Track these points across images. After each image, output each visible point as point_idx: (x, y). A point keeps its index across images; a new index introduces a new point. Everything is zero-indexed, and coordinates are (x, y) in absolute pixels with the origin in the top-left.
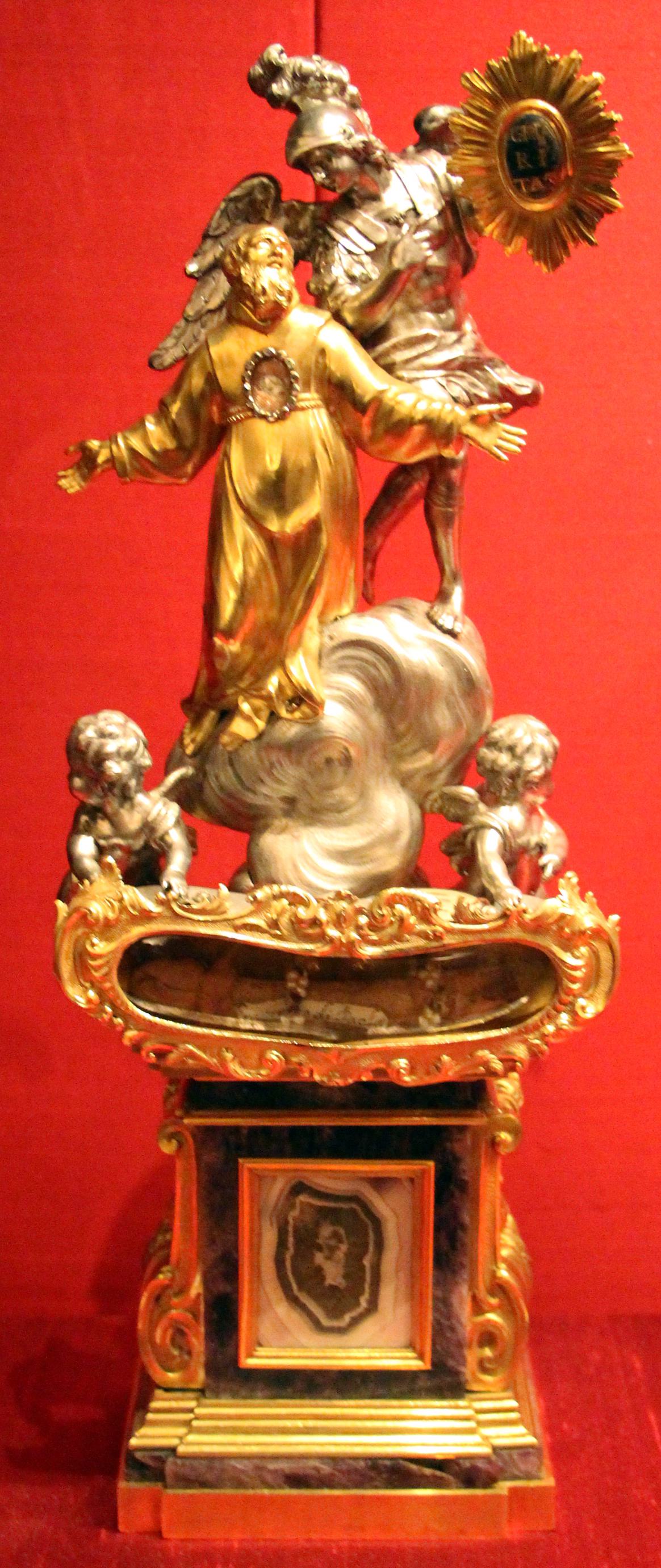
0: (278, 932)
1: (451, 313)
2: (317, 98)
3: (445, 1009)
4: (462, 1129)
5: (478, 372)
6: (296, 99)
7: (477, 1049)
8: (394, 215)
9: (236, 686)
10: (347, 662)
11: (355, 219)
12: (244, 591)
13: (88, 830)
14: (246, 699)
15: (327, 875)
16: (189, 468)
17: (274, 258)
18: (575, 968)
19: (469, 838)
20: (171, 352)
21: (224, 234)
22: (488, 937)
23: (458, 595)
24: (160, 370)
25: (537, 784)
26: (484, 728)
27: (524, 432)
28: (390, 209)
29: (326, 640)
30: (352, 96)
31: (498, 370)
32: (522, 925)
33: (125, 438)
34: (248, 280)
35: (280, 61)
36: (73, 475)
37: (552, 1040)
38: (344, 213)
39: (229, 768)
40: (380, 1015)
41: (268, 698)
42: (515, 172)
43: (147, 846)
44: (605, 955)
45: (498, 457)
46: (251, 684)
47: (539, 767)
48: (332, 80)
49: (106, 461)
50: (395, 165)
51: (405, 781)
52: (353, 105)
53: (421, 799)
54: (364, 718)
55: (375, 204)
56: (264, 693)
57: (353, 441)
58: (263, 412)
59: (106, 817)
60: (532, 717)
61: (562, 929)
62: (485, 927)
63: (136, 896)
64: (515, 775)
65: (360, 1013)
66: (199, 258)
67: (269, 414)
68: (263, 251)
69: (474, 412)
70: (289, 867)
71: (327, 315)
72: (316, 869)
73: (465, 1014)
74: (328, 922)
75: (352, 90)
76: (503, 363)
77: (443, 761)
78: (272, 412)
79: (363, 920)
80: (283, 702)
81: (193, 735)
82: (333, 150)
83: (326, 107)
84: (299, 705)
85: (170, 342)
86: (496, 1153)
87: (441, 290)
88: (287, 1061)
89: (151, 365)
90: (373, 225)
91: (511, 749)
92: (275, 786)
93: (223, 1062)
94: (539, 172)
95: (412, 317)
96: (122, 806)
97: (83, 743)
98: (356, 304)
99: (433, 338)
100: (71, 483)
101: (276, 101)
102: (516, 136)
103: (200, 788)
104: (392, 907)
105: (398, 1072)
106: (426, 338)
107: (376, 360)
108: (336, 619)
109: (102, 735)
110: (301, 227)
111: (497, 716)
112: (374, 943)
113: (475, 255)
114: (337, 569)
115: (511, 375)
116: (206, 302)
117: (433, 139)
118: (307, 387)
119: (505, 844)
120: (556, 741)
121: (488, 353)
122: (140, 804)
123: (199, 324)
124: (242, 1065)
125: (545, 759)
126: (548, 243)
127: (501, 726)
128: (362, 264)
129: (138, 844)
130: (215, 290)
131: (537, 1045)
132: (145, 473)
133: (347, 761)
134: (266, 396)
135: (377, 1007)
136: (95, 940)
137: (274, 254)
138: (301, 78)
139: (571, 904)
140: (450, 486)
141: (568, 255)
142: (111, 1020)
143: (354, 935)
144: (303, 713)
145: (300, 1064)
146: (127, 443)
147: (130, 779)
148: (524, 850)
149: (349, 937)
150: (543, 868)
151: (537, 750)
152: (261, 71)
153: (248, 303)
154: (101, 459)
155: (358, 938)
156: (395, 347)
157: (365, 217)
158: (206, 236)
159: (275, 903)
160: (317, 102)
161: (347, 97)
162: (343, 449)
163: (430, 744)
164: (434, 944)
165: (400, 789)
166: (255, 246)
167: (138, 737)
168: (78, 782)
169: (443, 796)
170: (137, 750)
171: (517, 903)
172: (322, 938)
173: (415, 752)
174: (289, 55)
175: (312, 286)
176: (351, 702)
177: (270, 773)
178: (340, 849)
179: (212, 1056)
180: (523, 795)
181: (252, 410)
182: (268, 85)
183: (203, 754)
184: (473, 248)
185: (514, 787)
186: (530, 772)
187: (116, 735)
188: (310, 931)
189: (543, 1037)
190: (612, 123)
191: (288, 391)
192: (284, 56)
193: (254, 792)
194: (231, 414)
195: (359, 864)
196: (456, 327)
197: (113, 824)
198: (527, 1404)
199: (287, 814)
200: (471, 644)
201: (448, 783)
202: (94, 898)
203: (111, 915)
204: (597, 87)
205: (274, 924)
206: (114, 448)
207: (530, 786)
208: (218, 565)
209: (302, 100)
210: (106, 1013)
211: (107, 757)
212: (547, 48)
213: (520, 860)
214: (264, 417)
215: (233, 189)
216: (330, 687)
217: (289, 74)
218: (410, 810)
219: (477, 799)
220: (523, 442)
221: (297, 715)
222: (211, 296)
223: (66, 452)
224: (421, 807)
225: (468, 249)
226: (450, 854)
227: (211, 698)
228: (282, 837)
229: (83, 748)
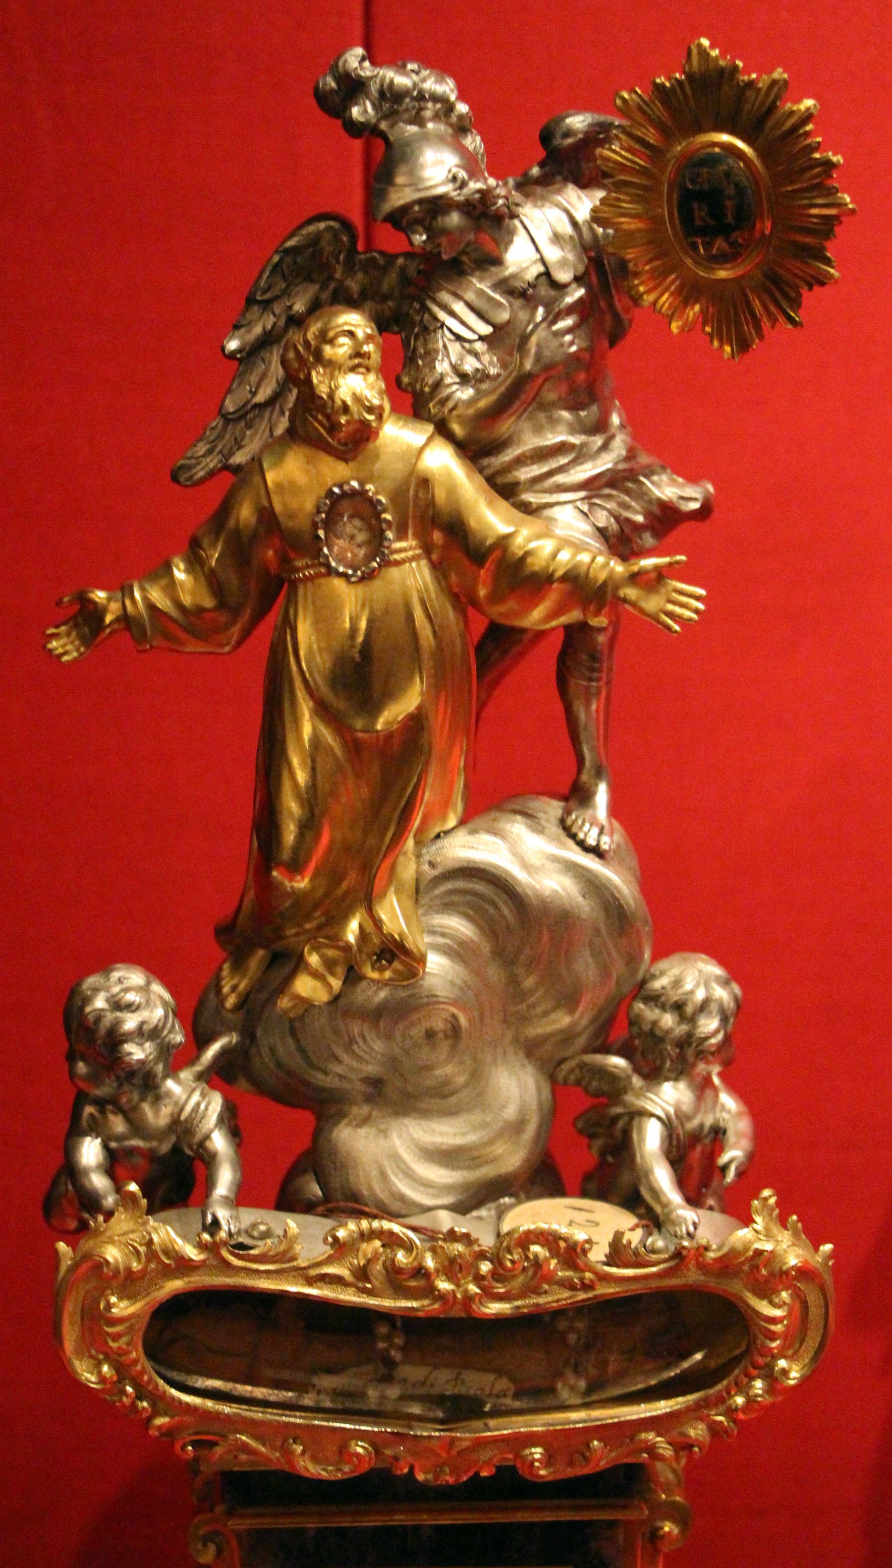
0: (369, 1286)
1: (594, 408)
2: (411, 122)
3: (593, 1372)
4: (612, 1524)
5: (630, 485)
6: (383, 126)
7: (641, 1431)
8: (519, 284)
9: (299, 925)
10: (455, 898)
11: (465, 292)
12: (311, 799)
13: (95, 1128)
14: (316, 948)
15: (426, 1184)
16: (236, 630)
17: (356, 361)
18: (774, 1320)
19: (621, 1124)
20: (203, 460)
21: (277, 298)
22: (654, 1284)
23: (602, 795)
24: (187, 486)
25: (713, 1054)
26: (641, 974)
27: (702, 592)
28: (514, 276)
29: (426, 867)
30: (461, 117)
31: (655, 478)
32: (702, 1267)
33: (143, 590)
34: (323, 390)
35: (362, 74)
36: (68, 634)
37: (741, 1416)
38: (449, 279)
39: (290, 1040)
40: (504, 1384)
41: (347, 948)
42: (690, 227)
43: (176, 1149)
44: (814, 1298)
45: (669, 628)
46: (320, 928)
47: (717, 1032)
48: (435, 98)
49: (117, 620)
50: (521, 210)
51: (531, 1049)
52: (461, 129)
53: (551, 1071)
54: (477, 972)
55: (493, 269)
56: (340, 944)
57: (463, 599)
58: (341, 569)
59: (120, 1110)
60: (704, 956)
61: (757, 1268)
62: (654, 1269)
63: (169, 1233)
64: (686, 1042)
65: (476, 1382)
66: (243, 330)
67: (350, 572)
68: (342, 349)
69: (635, 568)
70: (375, 1173)
71: (430, 428)
72: (409, 1175)
73: (620, 1376)
74: (437, 1271)
75: (462, 108)
76: (664, 468)
77: (584, 1022)
78: (355, 571)
79: (485, 1267)
80: (369, 956)
81: (235, 981)
82: (436, 206)
83: (425, 137)
84: (390, 962)
85: (201, 448)
86: (657, 1551)
87: (581, 386)
88: (378, 1452)
89: (175, 478)
90: (491, 299)
91: (678, 1007)
92: (355, 1064)
93: (288, 1454)
94: (724, 230)
95: (542, 416)
96: (143, 1099)
97: (91, 1018)
98: (471, 411)
99: (572, 447)
100: (64, 646)
101: (354, 129)
102: (693, 181)
103: (246, 1055)
104: (526, 1249)
105: (531, 1464)
106: (561, 448)
107: (491, 480)
108: (438, 836)
109: (118, 1005)
110: (385, 287)
111: (657, 956)
112: (500, 1298)
113: (627, 324)
114: (442, 784)
115: (673, 483)
116: (254, 394)
117: (567, 163)
118: (401, 535)
119: (670, 1136)
120: (736, 988)
121: (644, 459)
122: (169, 1094)
123: (243, 423)
124: (315, 1459)
125: (724, 1019)
126: (733, 318)
127: (662, 973)
128: (476, 355)
129: (165, 1148)
130: (264, 376)
131: (721, 1422)
132: (167, 636)
133: (454, 1031)
134: (344, 547)
135: (500, 1372)
136: (113, 1299)
137: (358, 354)
138: (391, 99)
139: (769, 1235)
140: (594, 657)
141: (761, 337)
142: (133, 1405)
143: (473, 1288)
144: (395, 971)
145: (396, 1458)
146: (148, 595)
147: (156, 1064)
148: (695, 1137)
149: (466, 1291)
150: (724, 1169)
151: (714, 1007)
152: (333, 84)
153: (320, 417)
154: (108, 618)
155: (478, 1291)
156: (520, 461)
157: (480, 285)
158: (251, 301)
159: (364, 1246)
160: (413, 129)
161: (454, 119)
162: (451, 614)
163: (569, 1000)
164: (582, 1296)
165: (526, 1062)
166: (331, 342)
167: (165, 1004)
168: (81, 1067)
169: (582, 1066)
170: (165, 1024)
171: (691, 1229)
172: (430, 1291)
173: (546, 1014)
174: (373, 63)
175: (406, 380)
176: (458, 951)
177: (348, 1049)
178: (444, 1147)
179: (273, 1448)
180: (694, 1065)
181: (328, 566)
182: (346, 108)
183: (252, 1011)
184: (625, 317)
185: (682, 1057)
186: (707, 1038)
187: (134, 999)
188: (413, 1283)
189: (731, 1412)
190: (829, 165)
191: (377, 543)
192: (367, 64)
193: (325, 1072)
194: (298, 570)
195: (469, 1168)
196: (600, 426)
197: (128, 1120)
198: (319, 784)
199: (369, 1099)
200: (621, 862)
201: (587, 1050)
202: (112, 1241)
203: (135, 1266)
204: (808, 117)
205: (362, 1274)
206: (128, 603)
207: (702, 1055)
208: (279, 777)
209: (392, 126)
210: (127, 1395)
211: (127, 1037)
212: (740, 64)
213: (694, 1154)
214: (344, 575)
215: (289, 237)
216: (432, 932)
217: (374, 88)
218: (539, 1089)
219: (630, 1072)
220: (701, 606)
221: (388, 974)
222: (258, 386)
223: (59, 603)
224: (552, 1078)
225: (617, 317)
226: (591, 1136)
227: (264, 934)
228: (362, 1131)
229: (91, 1025)
